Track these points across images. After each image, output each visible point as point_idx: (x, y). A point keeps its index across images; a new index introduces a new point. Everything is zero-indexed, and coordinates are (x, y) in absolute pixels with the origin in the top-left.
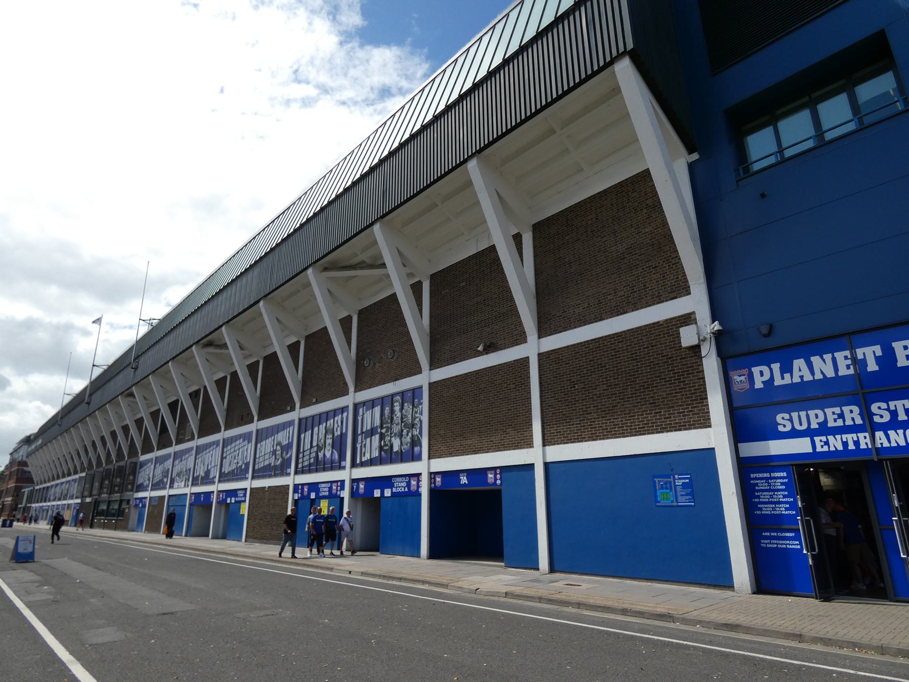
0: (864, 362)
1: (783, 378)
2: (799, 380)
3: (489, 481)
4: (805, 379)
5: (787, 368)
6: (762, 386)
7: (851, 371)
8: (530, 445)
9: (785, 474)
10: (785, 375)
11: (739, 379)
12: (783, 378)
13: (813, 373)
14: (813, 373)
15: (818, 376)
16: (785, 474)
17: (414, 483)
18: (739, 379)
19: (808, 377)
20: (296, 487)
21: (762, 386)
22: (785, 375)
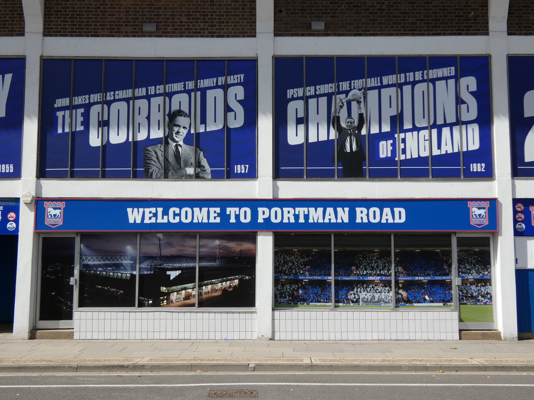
0: (229, 216)
1: (163, 218)
2: (385, 222)
3: (382, 155)
4: (389, 222)
5: (165, 213)
6: (262, 221)
7: (218, 220)
8: (251, 33)
9: (242, 81)
10: (165, 217)
11: (477, 212)
12: (163, 218)
13: (336, 218)
14: (336, 218)
15: (339, 221)
16: (242, 81)
17: (477, 167)
18: (477, 212)
19: (333, 221)
20: (39, 204)
21: (262, 221)
22: (165, 217)
